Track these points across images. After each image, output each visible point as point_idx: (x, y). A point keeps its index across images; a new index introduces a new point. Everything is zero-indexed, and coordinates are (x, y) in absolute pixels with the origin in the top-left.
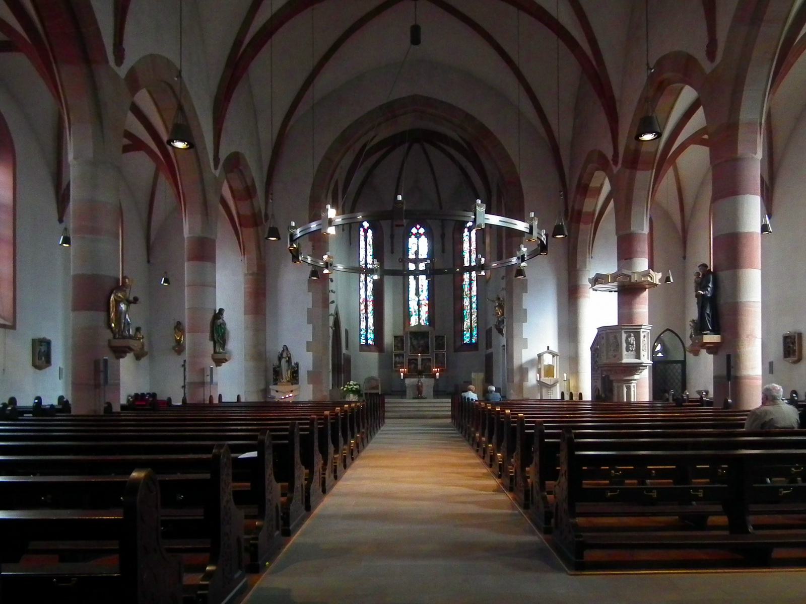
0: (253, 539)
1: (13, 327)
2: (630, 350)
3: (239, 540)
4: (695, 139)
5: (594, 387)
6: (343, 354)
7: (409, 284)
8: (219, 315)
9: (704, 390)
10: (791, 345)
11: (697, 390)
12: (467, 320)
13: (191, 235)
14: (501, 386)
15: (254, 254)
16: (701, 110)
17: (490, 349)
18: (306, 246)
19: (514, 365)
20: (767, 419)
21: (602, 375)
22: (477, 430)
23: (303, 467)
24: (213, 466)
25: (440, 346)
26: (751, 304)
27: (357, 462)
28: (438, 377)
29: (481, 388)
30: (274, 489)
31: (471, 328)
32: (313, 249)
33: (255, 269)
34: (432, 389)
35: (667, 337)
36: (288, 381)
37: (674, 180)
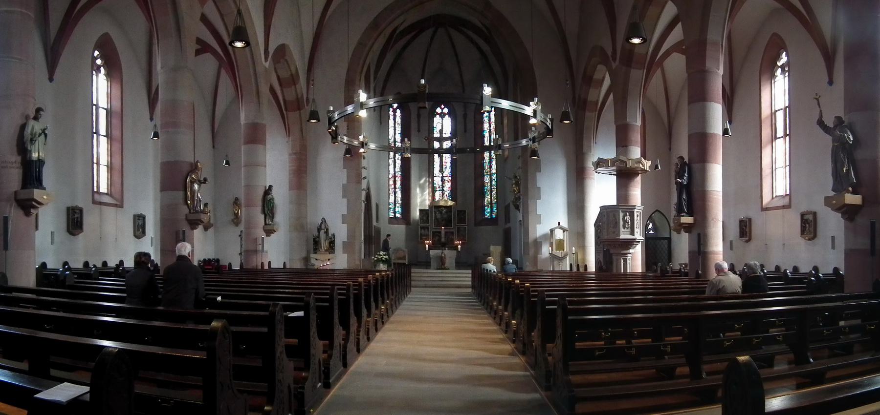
0: (300, 388)
1: (121, 206)
3: (289, 387)
4: (677, 48)
5: (597, 260)
6: (373, 227)
7: (434, 162)
8: (268, 191)
9: (684, 263)
10: (744, 228)
11: (680, 263)
13: (247, 122)
14: (518, 258)
16: (679, 26)
17: (508, 224)
18: (343, 127)
19: (530, 239)
20: (721, 287)
21: (603, 249)
22: (494, 298)
23: (341, 328)
24: (269, 321)
26: (715, 193)
27: (387, 326)
28: (459, 250)
29: (499, 259)
30: (318, 346)
32: (348, 129)
34: (454, 261)
35: (656, 216)
36: (326, 251)
37: (661, 79)
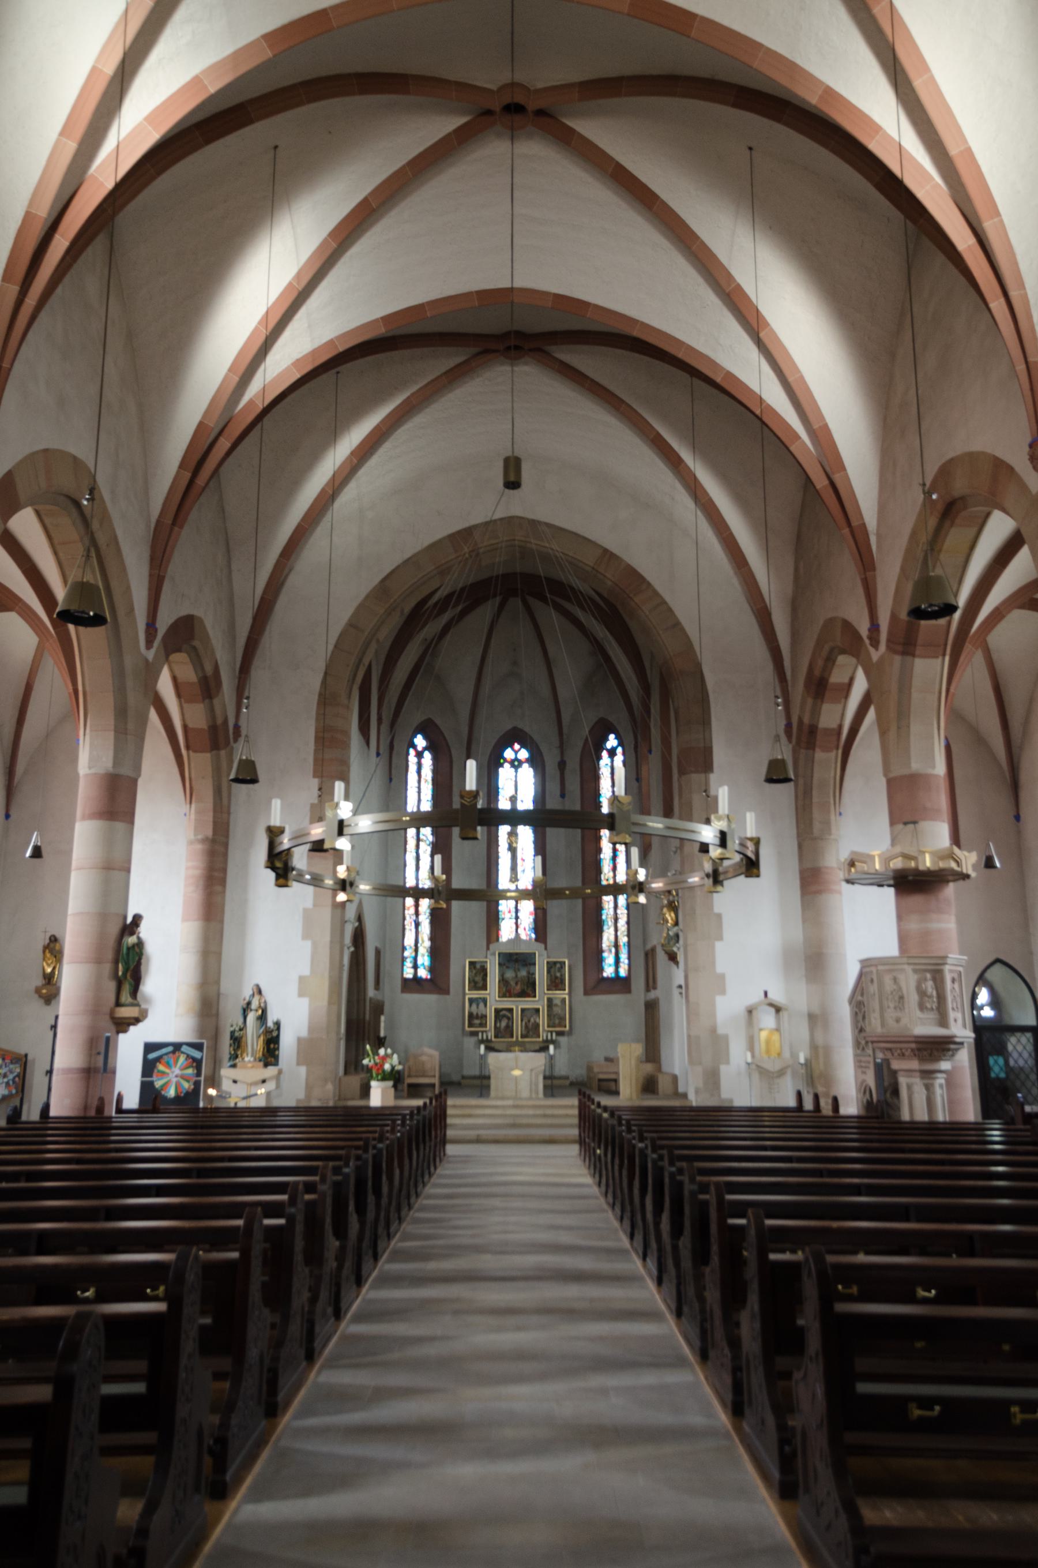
2: (926, 1008)
7: (497, 858)
12: (609, 929)
13: (93, 771)
15: (209, 803)
21: (875, 1058)
25: (556, 983)
31: (616, 945)
33: (209, 832)
35: (996, 974)
